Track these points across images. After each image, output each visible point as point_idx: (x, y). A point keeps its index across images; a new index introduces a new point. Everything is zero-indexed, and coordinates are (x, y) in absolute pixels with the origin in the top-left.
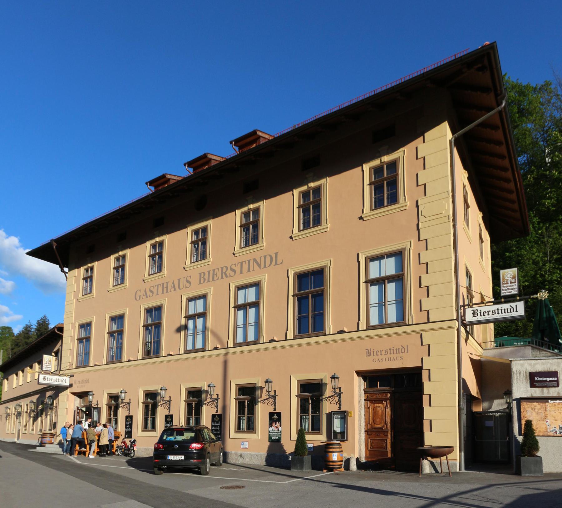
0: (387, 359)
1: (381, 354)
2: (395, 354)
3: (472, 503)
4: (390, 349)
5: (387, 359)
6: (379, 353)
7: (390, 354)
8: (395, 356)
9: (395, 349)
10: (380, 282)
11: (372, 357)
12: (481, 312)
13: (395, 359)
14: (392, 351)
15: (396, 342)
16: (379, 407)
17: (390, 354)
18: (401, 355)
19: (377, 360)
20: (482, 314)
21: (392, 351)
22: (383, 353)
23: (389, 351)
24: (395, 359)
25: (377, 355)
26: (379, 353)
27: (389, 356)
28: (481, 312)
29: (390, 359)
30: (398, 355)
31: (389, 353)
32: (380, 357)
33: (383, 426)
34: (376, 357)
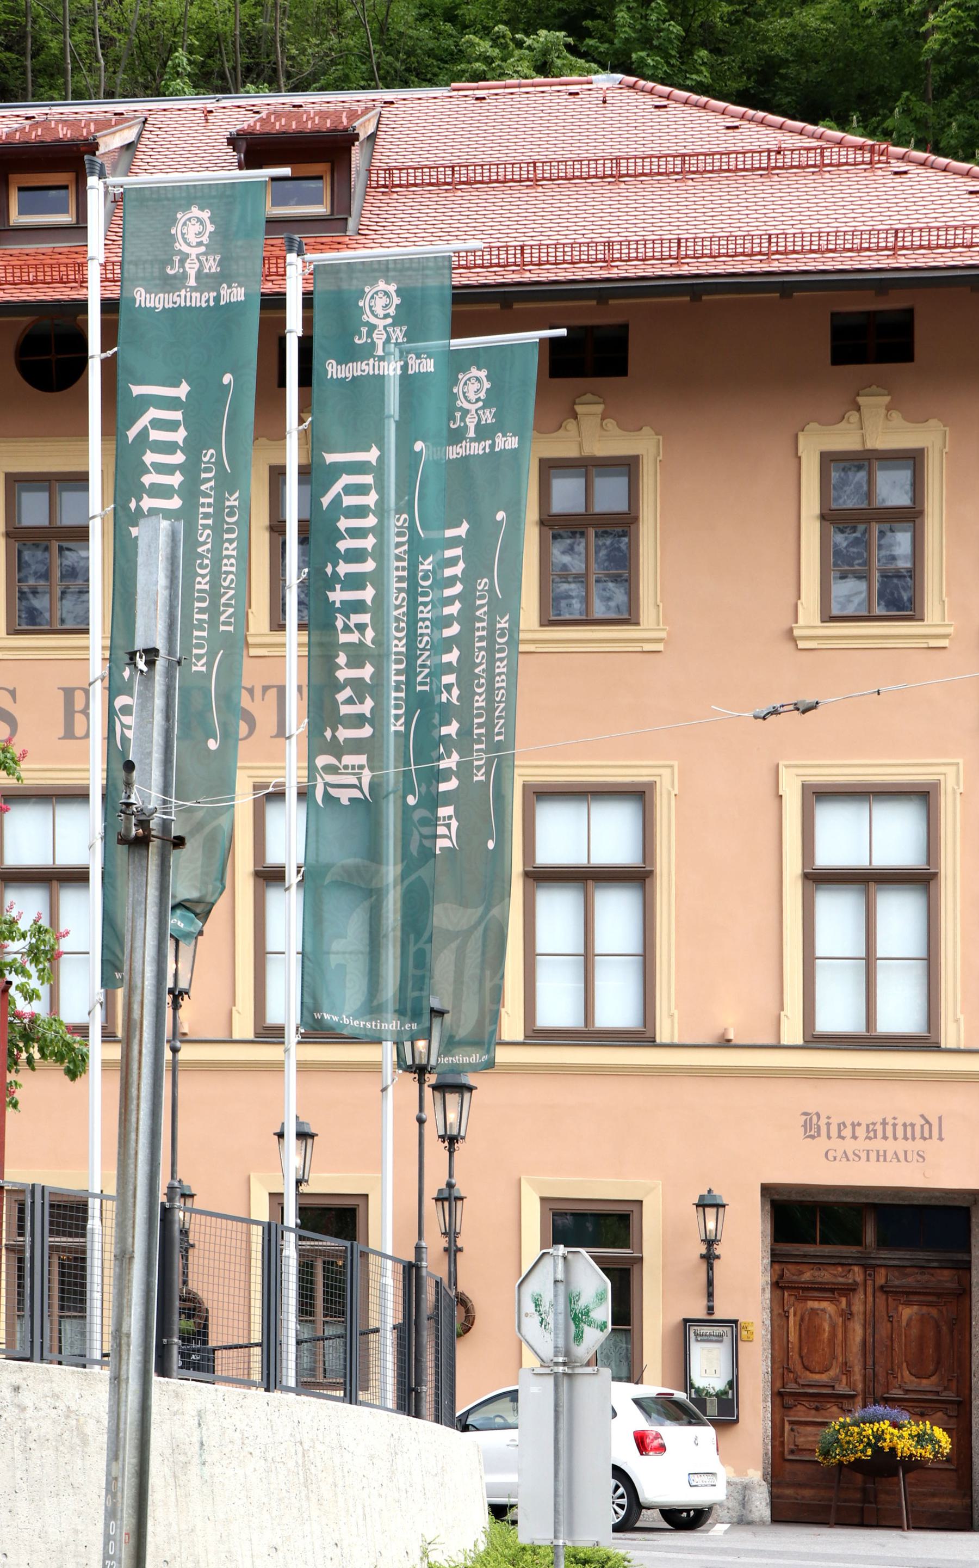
0: (873, 1156)
1: (854, 1137)
2: (900, 1140)
3: (110, 1289)
4: (884, 1123)
5: (873, 1156)
6: (847, 1132)
7: (885, 1137)
8: (900, 1146)
9: (900, 1122)
10: (867, 881)
11: (822, 1143)
12: (828, 1124)
13: (902, 1157)
14: (889, 1129)
15: (907, 1104)
16: (823, 1310)
17: (906, 1138)
18: (919, 1144)
19: (839, 1154)
20: (834, 1133)
21: (889, 1129)
22: (861, 1132)
23: (879, 1128)
24: (902, 1157)
25: (840, 1137)
26: (847, 1132)
27: (878, 1144)
28: (828, 1124)
29: (881, 1156)
30: (910, 1145)
31: (880, 1134)
32: (850, 1145)
33: (837, 1379)
34: (835, 1143)
